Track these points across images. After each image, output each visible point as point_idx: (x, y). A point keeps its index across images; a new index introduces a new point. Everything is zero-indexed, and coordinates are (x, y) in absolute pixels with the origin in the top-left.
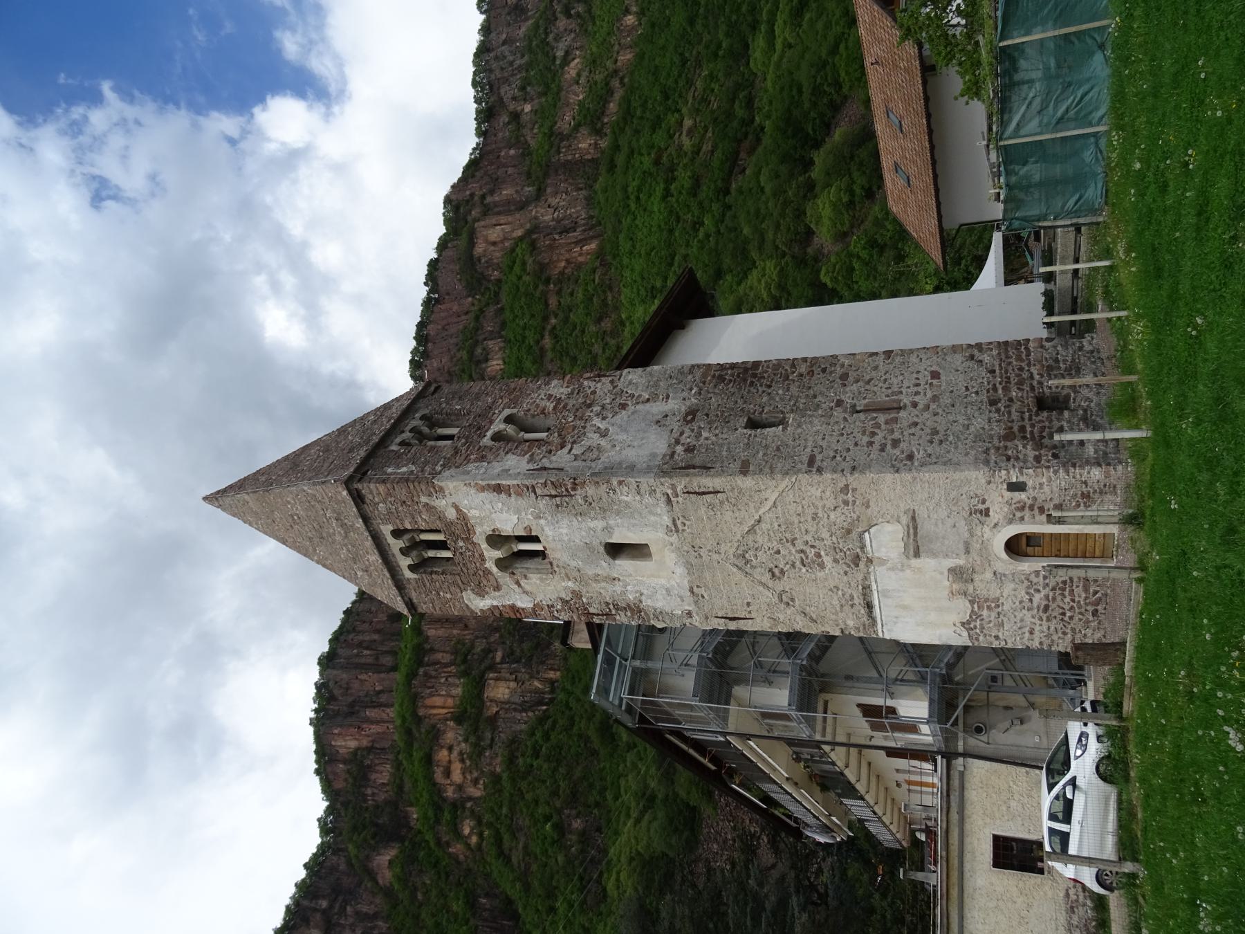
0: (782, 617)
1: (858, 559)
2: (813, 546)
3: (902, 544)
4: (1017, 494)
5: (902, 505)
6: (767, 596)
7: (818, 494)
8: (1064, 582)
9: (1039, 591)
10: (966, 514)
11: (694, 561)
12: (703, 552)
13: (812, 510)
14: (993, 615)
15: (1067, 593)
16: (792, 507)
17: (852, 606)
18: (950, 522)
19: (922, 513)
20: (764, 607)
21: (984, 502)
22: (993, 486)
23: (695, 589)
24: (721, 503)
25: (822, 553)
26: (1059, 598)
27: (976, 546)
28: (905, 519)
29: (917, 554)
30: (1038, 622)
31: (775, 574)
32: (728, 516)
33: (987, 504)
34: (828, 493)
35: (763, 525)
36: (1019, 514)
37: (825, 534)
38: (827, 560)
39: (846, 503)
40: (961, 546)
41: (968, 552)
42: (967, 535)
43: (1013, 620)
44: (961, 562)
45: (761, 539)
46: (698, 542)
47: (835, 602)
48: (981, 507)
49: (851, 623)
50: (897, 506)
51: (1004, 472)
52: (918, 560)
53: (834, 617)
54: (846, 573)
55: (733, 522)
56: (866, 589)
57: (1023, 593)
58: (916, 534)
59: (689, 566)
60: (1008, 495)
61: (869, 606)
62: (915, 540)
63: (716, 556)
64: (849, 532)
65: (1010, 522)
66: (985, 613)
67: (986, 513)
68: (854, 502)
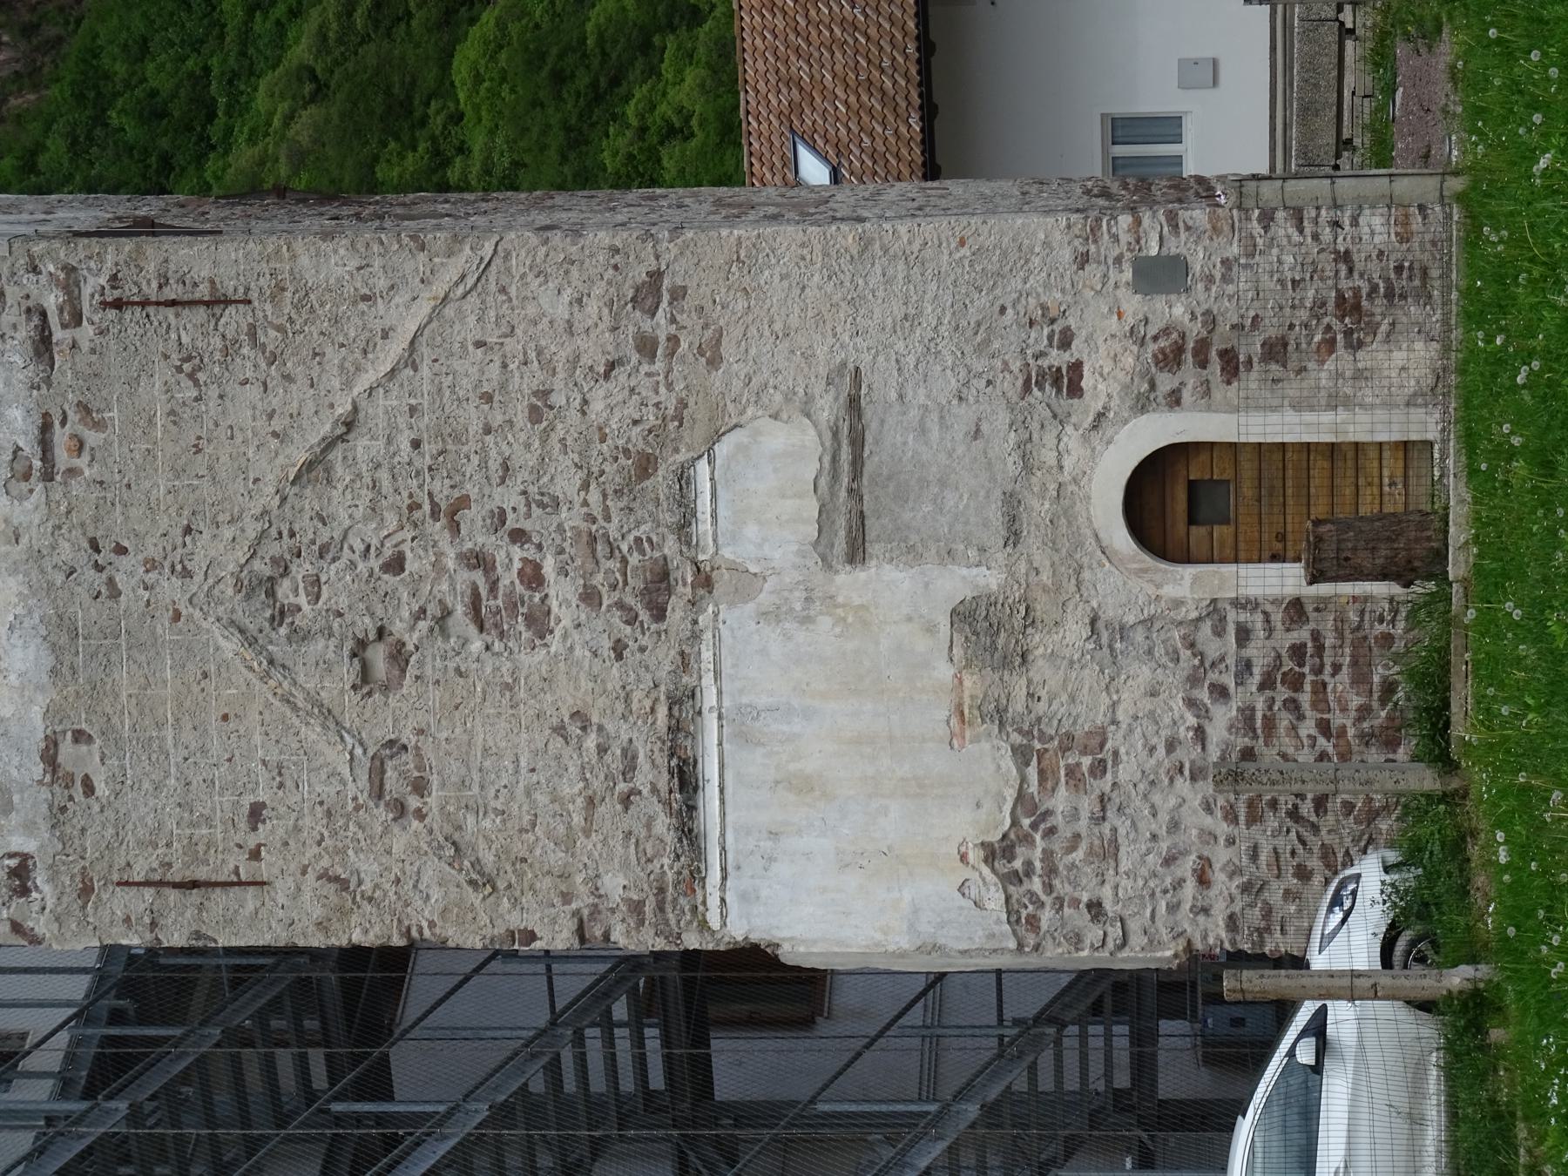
0: (368, 867)
1: (664, 588)
2: (518, 536)
3: (812, 508)
4: (1160, 302)
5: (821, 352)
6: (334, 767)
7: (562, 311)
8: (1298, 651)
9: (1221, 692)
10: (1010, 385)
11: (85, 612)
12: (127, 572)
13: (533, 379)
14: (1087, 805)
15: (1305, 698)
16: (468, 367)
17: (626, 801)
18: (964, 416)
19: (881, 385)
20: (313, 823)
21: (1066, 341)
22: (1093, 271)
23: (67, 750)
24: (230, 350)
25: (549, 567)
26: (1284, 720)
27: (1039, 508)
28: (828, 407)
29: (856, 553)
30: (1223, 829)
31: (376, 659)
32: (246, 404)
33: (1078, 349)
34: (592, 307)
35: (363, 446)
36: (1166, 382)
37: (566, 484)
38: (561, 593)
39: (647, 347)
40: (995, 513)
41: (1013, 536)
42: (1012, 466)
43: (1147, 826)
44: (990, 579)
45: (343, 504)
46: (116, 526)
47: (570, 788)
48: (1057, 358)
49: (614, 885)
50: (808, 357)
51: (1125, 220)
52: (861, 575)
53: (557, 858)
54: (619, 649)
55: (256, 428)
56: (683, 701)
57: (1178, 704)
58: (857, 473)
59: (63, 636)
60: (1133, 304)
61: (686, 779)
62: (855, 493)
63: (170, 589)
64: (646, 466)
65: (1142, 405)
66: (1060, 800)
67: (1070, 381)
68: (674, 340)
